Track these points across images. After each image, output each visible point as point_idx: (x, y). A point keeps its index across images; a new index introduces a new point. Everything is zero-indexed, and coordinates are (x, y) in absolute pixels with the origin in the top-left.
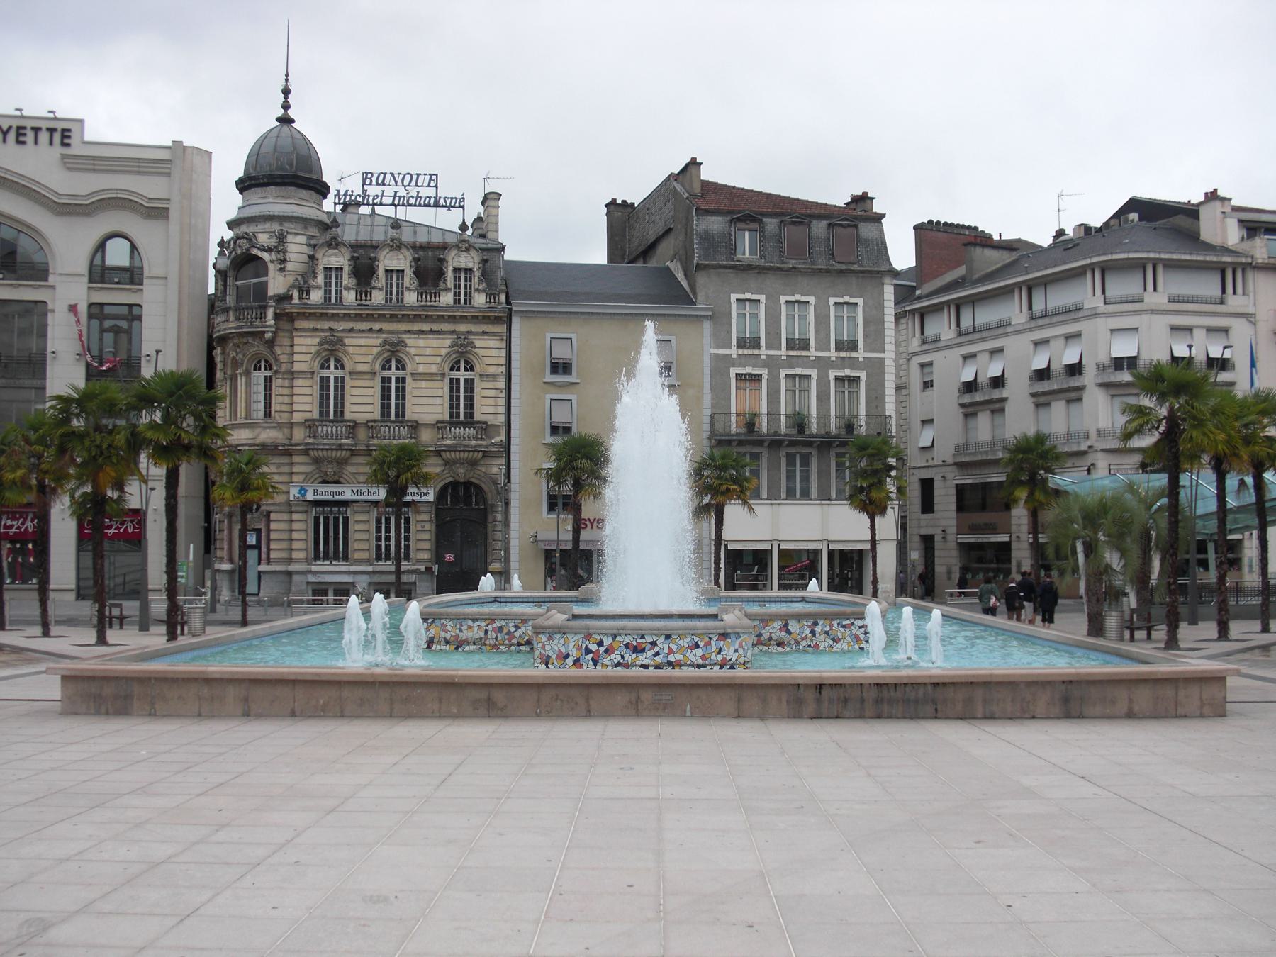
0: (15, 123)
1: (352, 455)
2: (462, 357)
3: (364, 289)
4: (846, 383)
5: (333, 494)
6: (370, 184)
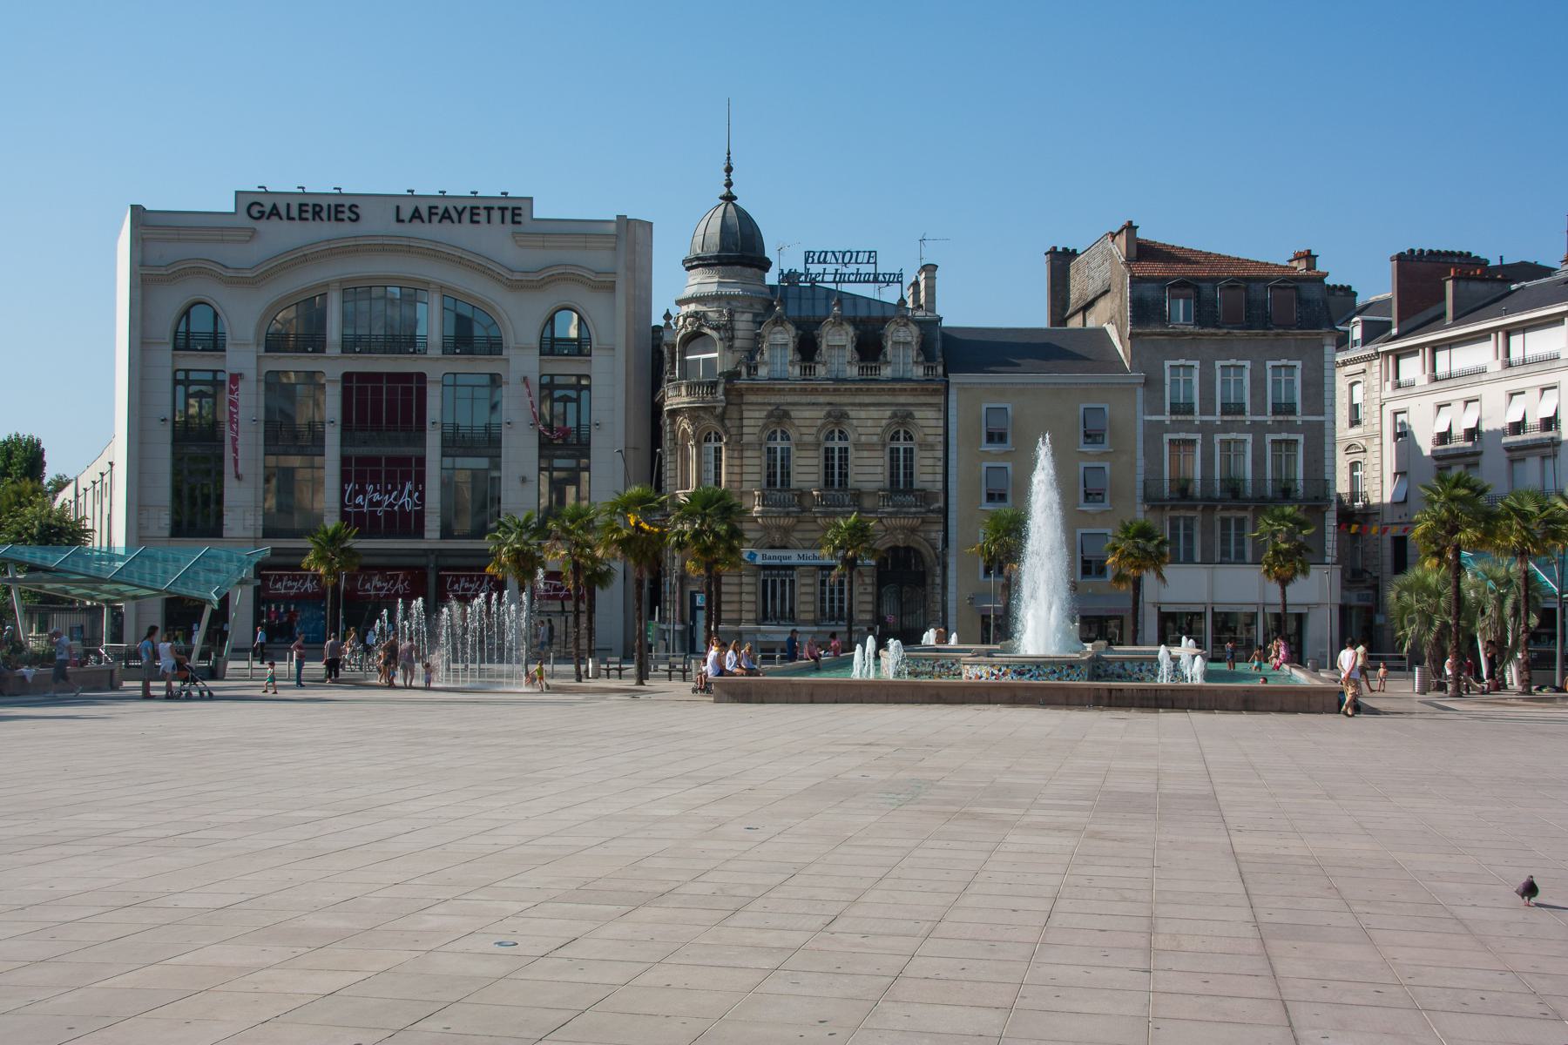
0: (469, 204)
1: (799, 522)
2: (902, 423)
3: (808, 364)
4: (1284, 445)
5: (780, 558)
6: (813, 262)
